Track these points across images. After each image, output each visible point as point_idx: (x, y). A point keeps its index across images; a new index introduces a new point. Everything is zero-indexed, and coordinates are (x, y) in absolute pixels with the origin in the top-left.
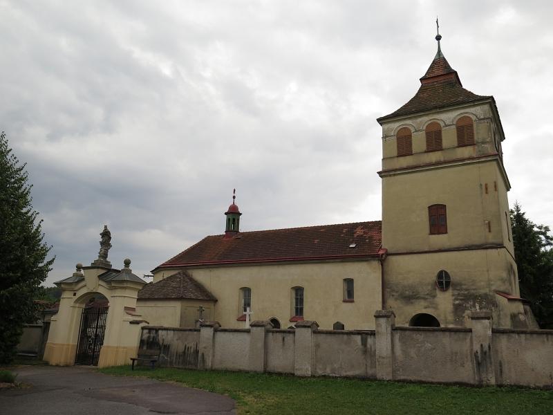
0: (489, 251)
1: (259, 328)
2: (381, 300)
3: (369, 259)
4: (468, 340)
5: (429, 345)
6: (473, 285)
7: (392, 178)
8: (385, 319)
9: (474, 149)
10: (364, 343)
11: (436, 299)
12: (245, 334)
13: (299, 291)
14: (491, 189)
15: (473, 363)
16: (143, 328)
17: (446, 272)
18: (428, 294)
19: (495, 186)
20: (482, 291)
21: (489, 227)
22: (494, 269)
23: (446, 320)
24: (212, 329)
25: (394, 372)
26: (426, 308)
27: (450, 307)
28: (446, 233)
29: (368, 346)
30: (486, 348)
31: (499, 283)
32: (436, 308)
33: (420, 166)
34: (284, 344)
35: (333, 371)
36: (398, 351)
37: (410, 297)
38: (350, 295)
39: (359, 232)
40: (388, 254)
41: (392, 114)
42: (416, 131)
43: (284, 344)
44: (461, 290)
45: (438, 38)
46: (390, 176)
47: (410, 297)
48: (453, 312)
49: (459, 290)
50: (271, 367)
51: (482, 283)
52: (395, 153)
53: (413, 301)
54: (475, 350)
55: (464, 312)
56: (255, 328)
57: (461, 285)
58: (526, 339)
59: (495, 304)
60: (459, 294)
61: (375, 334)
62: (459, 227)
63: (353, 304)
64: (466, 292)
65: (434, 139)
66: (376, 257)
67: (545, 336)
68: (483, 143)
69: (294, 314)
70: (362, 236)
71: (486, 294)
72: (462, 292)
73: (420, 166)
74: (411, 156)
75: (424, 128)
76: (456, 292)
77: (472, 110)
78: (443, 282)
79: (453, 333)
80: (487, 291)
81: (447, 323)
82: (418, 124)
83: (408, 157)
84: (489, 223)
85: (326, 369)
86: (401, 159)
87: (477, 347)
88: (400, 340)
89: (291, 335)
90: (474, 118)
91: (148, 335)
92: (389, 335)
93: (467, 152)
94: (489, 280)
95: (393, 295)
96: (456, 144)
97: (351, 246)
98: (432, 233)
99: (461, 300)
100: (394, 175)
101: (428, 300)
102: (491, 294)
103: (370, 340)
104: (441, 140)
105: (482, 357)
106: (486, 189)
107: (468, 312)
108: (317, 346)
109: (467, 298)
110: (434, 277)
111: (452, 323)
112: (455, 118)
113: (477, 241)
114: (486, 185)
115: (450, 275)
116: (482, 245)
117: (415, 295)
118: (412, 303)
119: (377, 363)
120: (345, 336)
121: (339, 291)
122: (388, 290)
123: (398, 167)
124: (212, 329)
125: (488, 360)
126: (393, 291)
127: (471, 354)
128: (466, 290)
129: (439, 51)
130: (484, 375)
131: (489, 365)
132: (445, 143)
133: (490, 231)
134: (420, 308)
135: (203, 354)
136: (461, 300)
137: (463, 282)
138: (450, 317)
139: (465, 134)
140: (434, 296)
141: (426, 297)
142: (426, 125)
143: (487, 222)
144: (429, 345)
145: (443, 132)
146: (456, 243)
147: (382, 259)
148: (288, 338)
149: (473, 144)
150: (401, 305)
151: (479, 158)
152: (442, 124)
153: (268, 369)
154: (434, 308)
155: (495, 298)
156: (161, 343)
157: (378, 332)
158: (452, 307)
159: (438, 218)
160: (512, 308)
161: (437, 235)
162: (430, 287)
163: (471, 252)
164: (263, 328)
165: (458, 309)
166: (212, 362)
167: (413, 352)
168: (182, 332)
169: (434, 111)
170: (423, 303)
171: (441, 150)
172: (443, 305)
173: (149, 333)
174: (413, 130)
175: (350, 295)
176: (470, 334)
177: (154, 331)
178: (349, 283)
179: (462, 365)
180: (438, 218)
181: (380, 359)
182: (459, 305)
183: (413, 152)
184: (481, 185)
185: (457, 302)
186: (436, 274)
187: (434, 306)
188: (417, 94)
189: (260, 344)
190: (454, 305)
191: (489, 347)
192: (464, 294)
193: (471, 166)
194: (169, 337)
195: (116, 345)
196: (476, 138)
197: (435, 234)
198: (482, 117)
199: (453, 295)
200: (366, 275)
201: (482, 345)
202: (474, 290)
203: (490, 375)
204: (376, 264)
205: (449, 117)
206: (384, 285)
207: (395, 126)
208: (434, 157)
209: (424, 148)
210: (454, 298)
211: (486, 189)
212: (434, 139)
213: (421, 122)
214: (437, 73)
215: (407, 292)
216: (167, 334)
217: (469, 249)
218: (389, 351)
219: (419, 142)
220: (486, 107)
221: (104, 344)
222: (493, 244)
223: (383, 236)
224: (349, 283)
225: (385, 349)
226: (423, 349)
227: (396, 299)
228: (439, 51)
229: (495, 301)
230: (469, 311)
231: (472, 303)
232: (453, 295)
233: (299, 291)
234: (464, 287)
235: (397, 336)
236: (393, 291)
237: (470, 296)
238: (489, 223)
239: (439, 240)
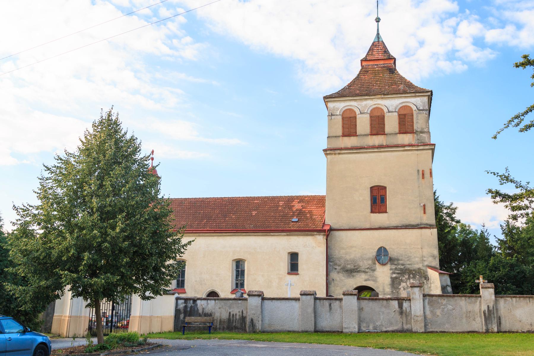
0: (424, 231)
1: (309, 297)
2: (325, 273)
3: (315, 233)
4: (478, 303)
5: (450, 307)
6: (408, 260)
7: (337, 156)
8: (418, 288)
9: (413, 137)
10: (401, 306)
11: (376, 273)
12: (293, 302)
13: (239, 264)
14: (427, 175)
15: (481, 318)
16: (177, 299)
17: (385, 249)
18: (368, 268)
19: (431, 173)
20: (416, 266)
21: (424, 209)
22: (422, 247)
23: (384, 291)
24: (260, 298)
25: (425, 326)
26: (366, 280)
27: (388, 281)
28: (386, 212)
29: (404, 309)
30: (491, 308)
31: (431, 259)
32: (375, 281)
33: (364, 148)
34: (330, 309)
35: (375, 328)
36: (428, 312)
37: (352, 271)
38: (294, 268)
39: (297, 206)
40: (331, 230)
41: (337, 93)
42: (361, 113)
43: (330, 309)
44: (398, 264)
45: (378, 20)
46: (335, 154)
47: (352, 271)
48: (390, 285)
49: (395, 265)
50: (319, 328)
51: (417, 259)
52: (340, 132)
53: (355, 274)
54: (483, 309)
55: (400, 285)
56: (304, 297)
57: (398, 260)
58: (516, 301)
59: (427, 278)
60: (396, 269)
61: (410, 300)
62: (398, 208)
63: (297, 276)
64: (402, 267)
65: (378, 124)
66: (319, 231)
67: (528, 299)
68: (422, 132)
69: (234, 287)
70: (301, 210)
71: (419, 269)
72: (399, 267)
73: (364, 148)
74: (355, 137)
75: (369, 112)
76: (394, 267)
77: (413, 100)
78: (382, 255)
79: (467, 298)
80: (420, 266)
81: (384, 294)
82: (363, 107)
83: (352, 138)
84: (424, 205)
85: (369, 327)
86: (346, 139)
87: (484, 307)
88: (428, 303)
89: (338, 302)
90: (414, 108)
91: (184, 305)
92: (422, 300)
93: (407, 139)
94: (423, 257)
95: (336, 269)
96: (397, 130)
97: (293, 220)
98: (372, 212)
99: (398, 273)
100: (339, 154)
101: (369, 273)
102: (424, 268)
103: (405, 305)
104: (384, 124)
105: (489, 314)
106: (423, 174)
107: (403, 284)
108: (361, 309)
109: (404, 272)
110: (374, 253)
111: (389, 295)
112: (398, 106)
113: (414, 222)
114: (423, 171)
115: (388, 250)
116: (418, 225)
117: (357, 269)
118: (353, 276)
119: (413, 321)
120: (385, 302)
121: (284, 264)
122: (331, 264)
123: (343, 146)
124: (260, 298)
125: (492, 315)
126: (336, 264)
127: (480, 311)
128: (403, 265)
129: (378, 34)
130: (490, 326)
131: (493, 319)
132: (388, 129)
133: (425, 213)
134: (360, 280)
135: (252, 320)
136: (398, 273)
137: (400, 258)
138: (388, 289)
139: (406, 122)
140: (374, 270)
141: (367, 270)
142: (371, 108)
143: (422, 204)
144: (450, 307)
145: (386, 117)
146: (394, 223)
147: (328, 232)
148: (335, 304)
149: (412, 132)
150: (343, 278)
151: (418, 146)
152: (386, 110)
153: (317, 329)
154: (374, 281)
155: (427, 272)
156: (200, 311)
157: (413, 298)
158: (390, 280)
159: (378, 199)
160: (436, 282)
161: (378, 214)
162: (370, 262)
163: (407, 231)
164: (313, 296)
165: (395, 283)
166: (262, 324)
167: (438, 312)
168: (224, 301)
169: (379, 96)
170: (363, 276)
171: (384, 134)
172: (382, 278)
173: (185, 302)
174: (358, 112)
175: (294, 268)
176: (479, 298)
177: (191, 301)
178: (294, 257)
179: (474, 320)
180: (378, 199)
181: (416, 318)
182: (396, 278)
183: (358, 134)
184: (418, 171)
185: (394, 276)
186: (376, 250)
187: (373, 278)
188: (358, 75)
189: (310, 310)
190: (391, 278)
191: (493, 307)
192: (401, 269)
193: (410, 152)
194: (209, 306)
195: (149, 315)
196: (415, 127)
197: (376, 213)
198: (421, 108)
199: (391, 269)
200: (311, 248)
201: (488, 306)
202: (409, 264)
203: (494, 325)
204: (321, 239)
205: (391, 104)
206: (329, 259)
207: (340, 106)
208: (378, 140)
209: (368, 131)
210: (391, 271)
211: (423, 174)
212: (378, 124)
213: (366, 105)
214: (376, 56)
215: (349, 266)
216: (208, 304)
217: (397, 229)
218: (422, 312)
219: (363, 124)
220: (426, 99)
221: (132, 315)
222: (427, 224)
223: (326, 209)
224: (294, 257)
225: (419, 310)
226: (446, 309)
227: (338, 272)
228: (378, 34)
229: (427, 275)
230: (404, 284)
231: (407, 277)
232: (391, 269)
233: (239, 264)
234: (401, 262)
235: (427, 301)
236: (336, 264)
237: (406, 270)
238: (424, 205)
239: (379, 219)
